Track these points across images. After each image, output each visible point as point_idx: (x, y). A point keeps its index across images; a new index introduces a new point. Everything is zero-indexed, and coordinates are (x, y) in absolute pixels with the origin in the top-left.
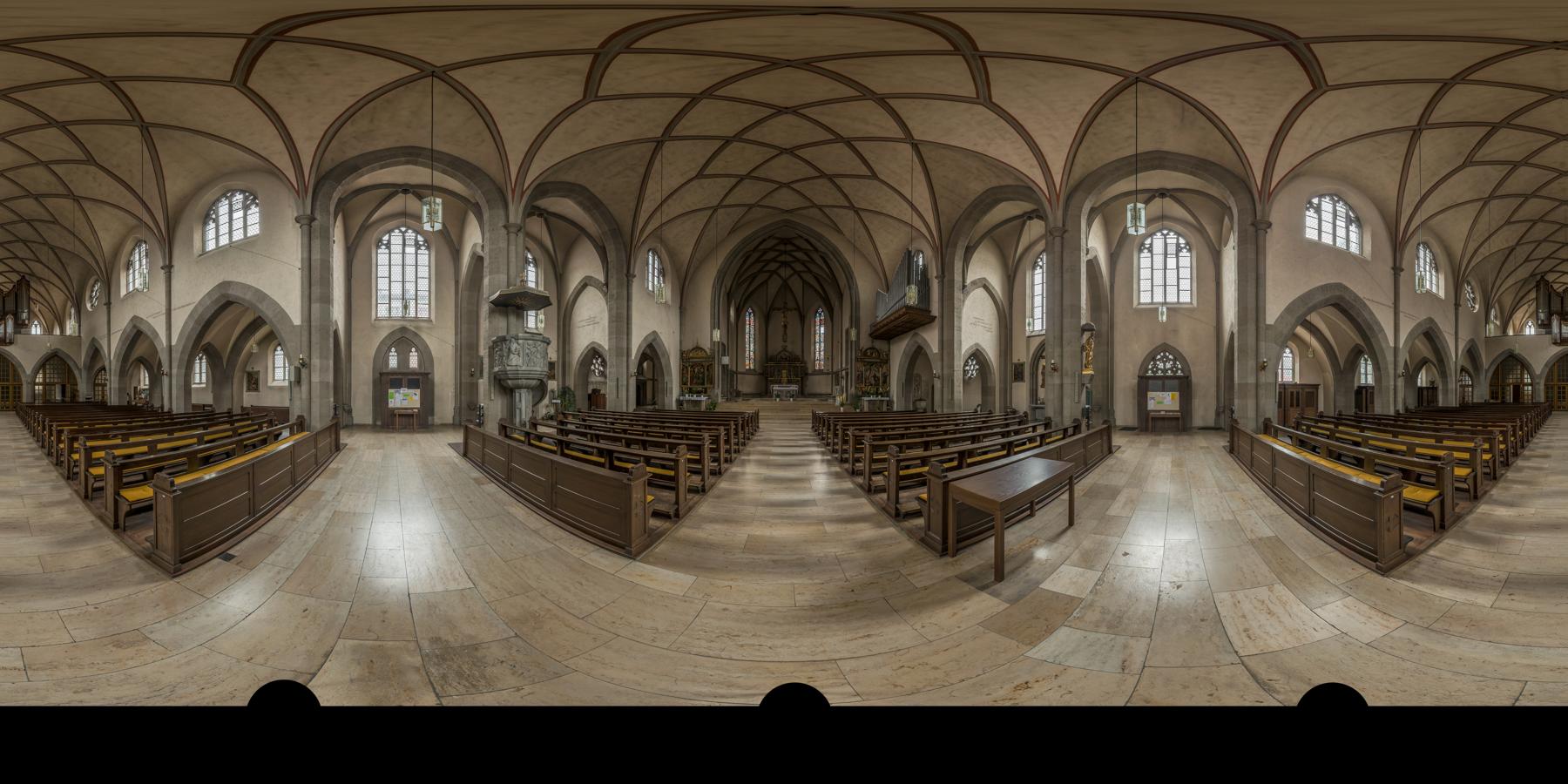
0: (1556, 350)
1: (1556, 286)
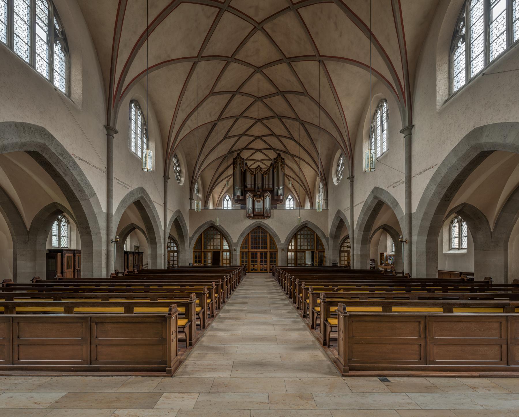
0: (249, 223)
1: (249, 163)
